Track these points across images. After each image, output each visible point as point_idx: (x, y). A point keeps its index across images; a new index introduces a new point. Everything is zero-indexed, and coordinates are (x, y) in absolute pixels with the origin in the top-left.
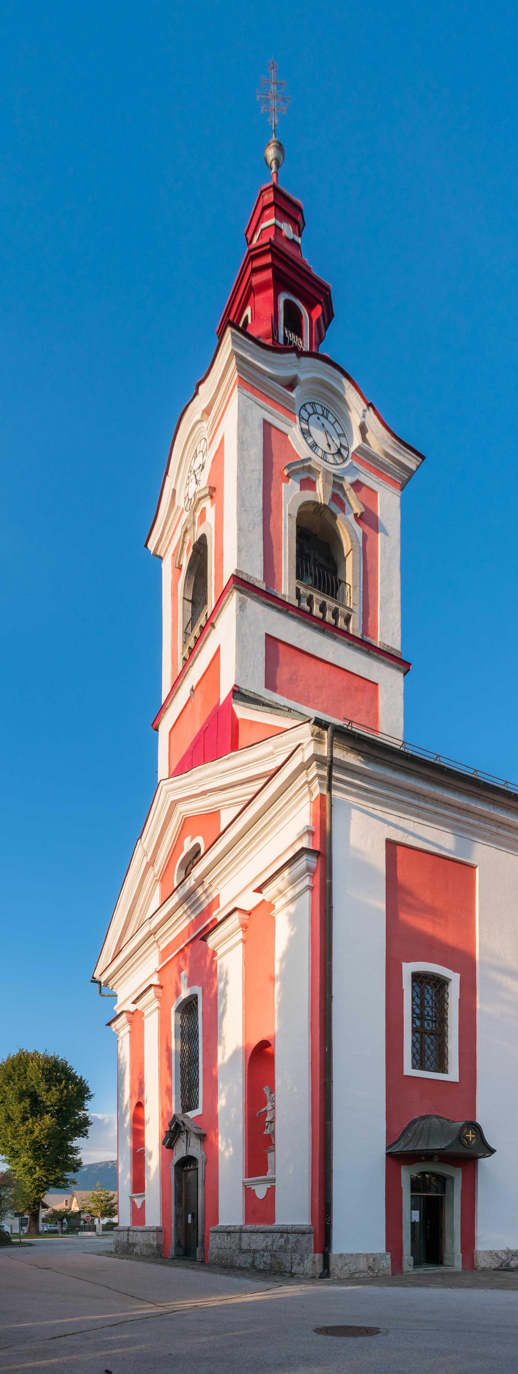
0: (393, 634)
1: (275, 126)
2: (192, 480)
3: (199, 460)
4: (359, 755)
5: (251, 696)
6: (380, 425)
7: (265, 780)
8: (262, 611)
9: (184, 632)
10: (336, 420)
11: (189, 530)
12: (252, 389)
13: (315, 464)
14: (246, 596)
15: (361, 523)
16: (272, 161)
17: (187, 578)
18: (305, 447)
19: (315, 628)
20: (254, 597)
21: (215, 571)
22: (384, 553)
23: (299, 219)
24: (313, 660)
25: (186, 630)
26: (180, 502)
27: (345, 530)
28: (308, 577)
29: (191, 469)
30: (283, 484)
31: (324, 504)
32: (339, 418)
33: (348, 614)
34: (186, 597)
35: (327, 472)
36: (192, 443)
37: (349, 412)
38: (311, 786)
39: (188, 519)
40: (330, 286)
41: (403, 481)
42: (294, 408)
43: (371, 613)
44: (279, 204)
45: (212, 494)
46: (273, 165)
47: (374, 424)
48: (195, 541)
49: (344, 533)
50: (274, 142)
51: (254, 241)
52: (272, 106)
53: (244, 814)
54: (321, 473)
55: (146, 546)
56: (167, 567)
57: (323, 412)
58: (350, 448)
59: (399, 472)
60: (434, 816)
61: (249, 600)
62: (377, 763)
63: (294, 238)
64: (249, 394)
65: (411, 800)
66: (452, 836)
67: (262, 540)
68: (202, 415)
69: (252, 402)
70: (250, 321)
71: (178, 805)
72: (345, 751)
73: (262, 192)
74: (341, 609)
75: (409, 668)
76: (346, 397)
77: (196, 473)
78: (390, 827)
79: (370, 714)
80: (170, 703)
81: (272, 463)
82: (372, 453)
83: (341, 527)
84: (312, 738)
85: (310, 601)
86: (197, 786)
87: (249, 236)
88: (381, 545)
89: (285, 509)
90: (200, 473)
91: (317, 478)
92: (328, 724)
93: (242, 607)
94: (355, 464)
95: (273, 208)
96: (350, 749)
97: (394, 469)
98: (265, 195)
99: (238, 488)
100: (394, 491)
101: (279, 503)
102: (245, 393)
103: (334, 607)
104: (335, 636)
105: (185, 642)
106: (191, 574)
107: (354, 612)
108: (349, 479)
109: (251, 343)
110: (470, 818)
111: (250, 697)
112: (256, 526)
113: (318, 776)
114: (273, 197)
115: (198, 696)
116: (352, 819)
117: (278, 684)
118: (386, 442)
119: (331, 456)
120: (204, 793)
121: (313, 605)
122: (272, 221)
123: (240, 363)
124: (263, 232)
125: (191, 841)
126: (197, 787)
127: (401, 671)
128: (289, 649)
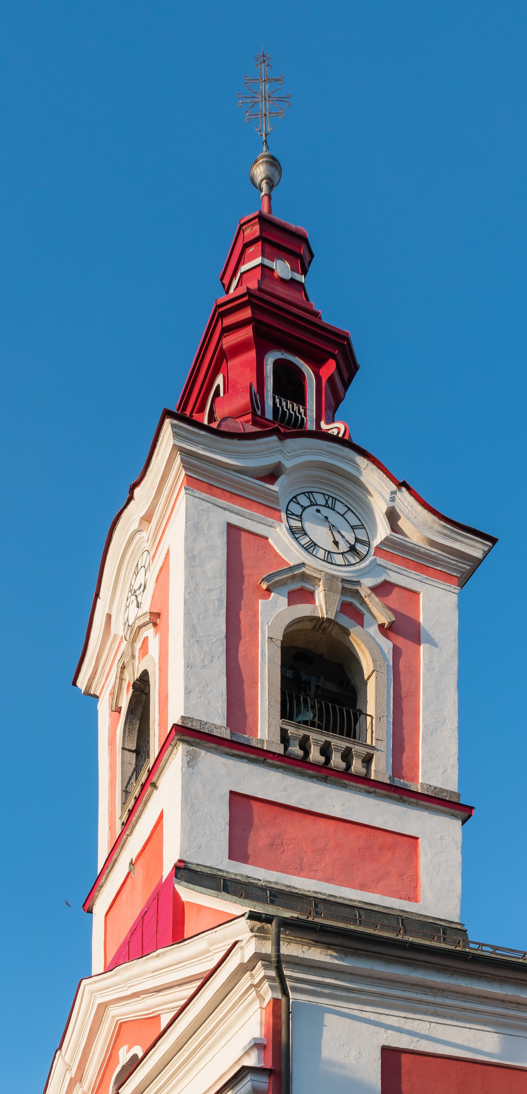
1: (266, 135)
2: (132, 601)
3: (140, 579)
4: (329, 948)
5: (205, 872)
6: (419, 508)
7: (198, 983)
9: (124, 791)
10: (349, 509)
11: (126, 666)
12: (210, 488)
13: (312, 569)
14: (198, 748)
15: (391, 634)
16: (262, 181)
17: (128, 724)
18: (297, 550)
19: (311, 777)
20: (211, 748)
21: (160, 716)
22: (429, 669)
23: (303, 251)
24: (309, 818)
25: (126, 787)
26: (118, 629)
27: (363, 646)
28: (308, 711)
29: (132, 588)
30: (260, 600)
31: (327, 618)
32: (354, 506)
33: (367, 753)
34: (126, 747)
35: (331, 578)
36: (131, 556)
37: (369, 497)
38: (259, 989)
39: (125, 652)
40: (348, 334)
42: (278, 504)
43: (407, 748)
44: (269, 237)
45: (155, 621)
46: (264, 185)
47: (409, 508)
48: (135, 679)
49: (362, 651)
50: (264, 157)
51: (232, 291)
52: (261, 111)
53: (177, 1024)
54: (322, 580)
55: (74, 683)
56: (104, 708)
57: (327, 501)
58: (371, 542)
59: (455, 562)
60: (462, 1013)
61: (203, 752)
62: (359, 956)
63: (293, 277)
64: (203, 495)
65: (420, 997)
66: (496, 1035)
67: (225, 675)
68: (140, 524)
69: (209, 504)
70: (222, 394)
71: (109, 1008)
72: (306, 945)
73: (241, 226)
74: (356, 748)
75: (471, 813)
76: (363, 479)
77: (137, 593)
78: (389, 1032)
79: (405, 877)
80: (106, 880)
81: (242, 577)
82: (408, 544)
83: (358, 644)
84: (251, 934)
85: (304, 744)
86: (126, 986)
87: (226, 282)
88: (424, 659)
90: (142, 593)
91: (316, 587)
92: (271, 917)
93: (191, 762)
94: (380, 561)
95: (260, 243)
96: (313, 943)
97: (447, 560)
98: (246, 229)
99: (185, 614)
100: (448, 588)
101: (254, 625)
102: (197, 495)
104: (344, 783)
105: (124, 804)
106: (133, 718)
107: (378, 750)
108: (368, 582)
109: (203, 433)
110: (523, 1011)
111: (203, 872)
112: (215, 659)
113: (265, 977)
114: (258, 230)
115: (139, 871)
116: (326, 1026)
117: (250, 852)
118: (432, 528)
119: (341, 556)
120: (136, 995)
121: (310, 748)
122: (258, 261)
123: (188, 459)
124: (244, 276)
125: (128, 1051)
126: (126, 988)
127: (458, 818)
128: (269, 806)
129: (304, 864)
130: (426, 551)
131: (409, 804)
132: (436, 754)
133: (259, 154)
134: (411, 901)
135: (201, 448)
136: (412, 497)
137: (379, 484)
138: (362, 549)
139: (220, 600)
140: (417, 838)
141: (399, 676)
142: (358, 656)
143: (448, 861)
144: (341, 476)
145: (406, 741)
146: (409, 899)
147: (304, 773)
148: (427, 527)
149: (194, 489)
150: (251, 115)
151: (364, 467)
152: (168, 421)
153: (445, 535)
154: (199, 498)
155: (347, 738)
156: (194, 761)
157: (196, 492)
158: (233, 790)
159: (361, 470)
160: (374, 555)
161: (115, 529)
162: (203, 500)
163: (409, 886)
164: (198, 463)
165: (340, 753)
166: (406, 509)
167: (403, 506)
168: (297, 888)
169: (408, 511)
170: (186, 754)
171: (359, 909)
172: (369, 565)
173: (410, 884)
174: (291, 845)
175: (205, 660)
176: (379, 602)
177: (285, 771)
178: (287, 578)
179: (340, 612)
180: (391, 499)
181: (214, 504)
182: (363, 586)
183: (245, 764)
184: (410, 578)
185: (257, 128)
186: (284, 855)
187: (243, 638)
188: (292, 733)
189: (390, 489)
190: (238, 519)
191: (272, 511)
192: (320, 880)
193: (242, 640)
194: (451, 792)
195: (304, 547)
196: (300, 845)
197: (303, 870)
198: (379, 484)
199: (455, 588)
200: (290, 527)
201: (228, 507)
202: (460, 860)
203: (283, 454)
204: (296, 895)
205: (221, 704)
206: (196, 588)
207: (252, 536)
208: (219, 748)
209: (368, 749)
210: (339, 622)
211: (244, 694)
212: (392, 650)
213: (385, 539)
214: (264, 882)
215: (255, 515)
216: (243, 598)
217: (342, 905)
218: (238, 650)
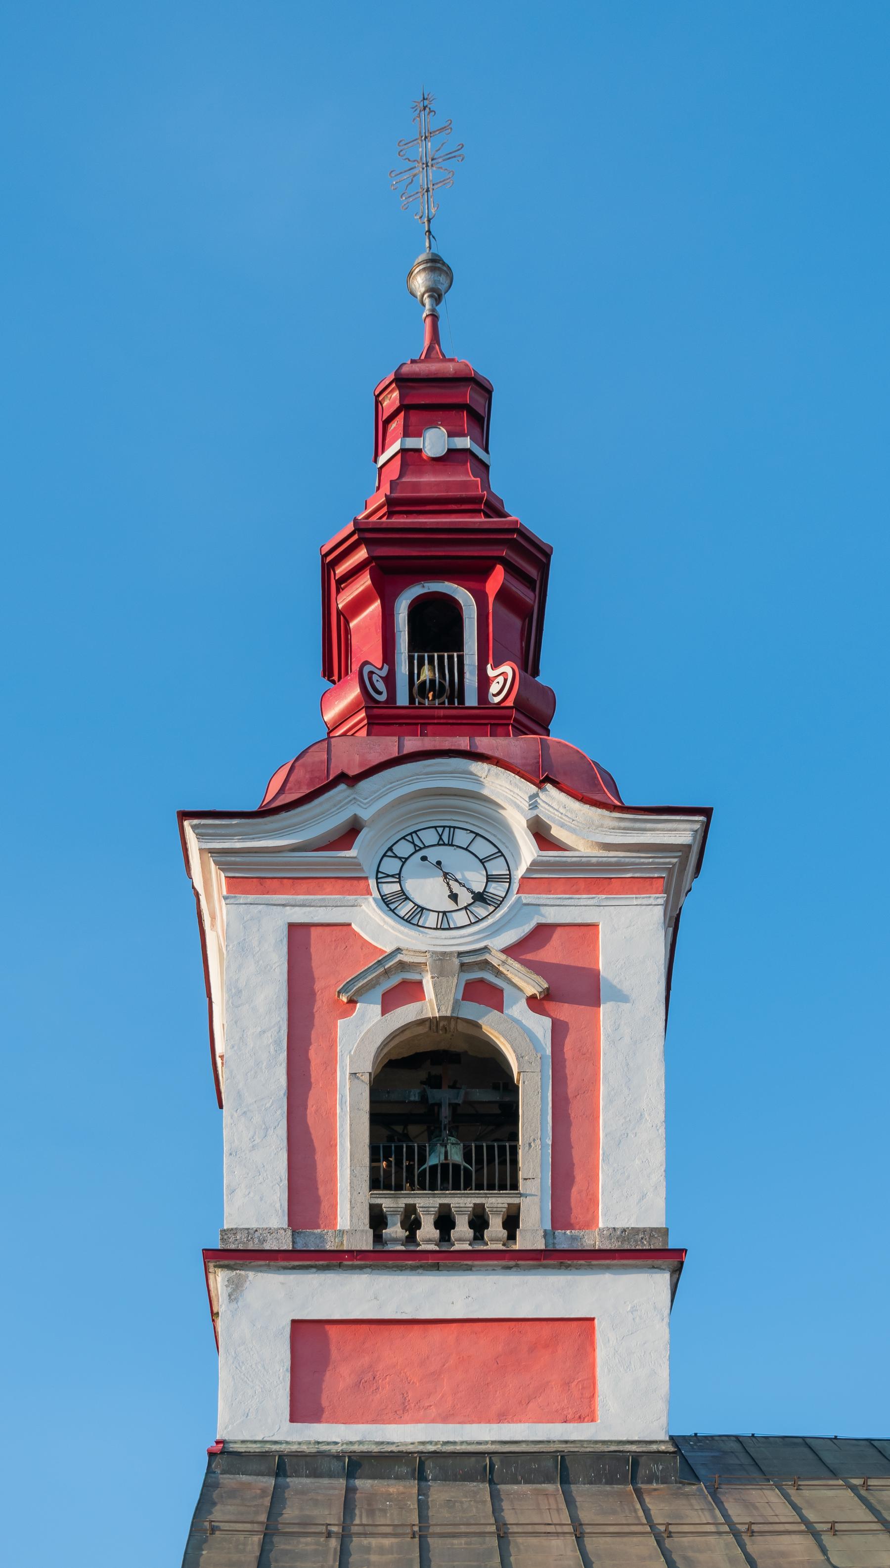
0: (644, 1196)
1: (429, 221)
8: (282, 1284)
10: (477, 834)
14: (243, 1270)
16: (423, 295)
18: (393, 928)
19: (414, 1268)
20: (260, 1266)
24: (416, 1327)
35: (442, 957)
37: (501, 811)
41: (670, 871)
42: (362, 870)
43: (579, 1175)
47: (562, 810)
59: (651, 860)
61: (251, 1274)
64: (251, 898)
69: (260, 907)
73: (377, 397)
76: (486, 792)
81: (313, 994)
89: (342, 1068)
94: (526, 898)
97: (637, 860)
98: (384, 399)
100: (645, 902)
101: (330, 1063)
102: (241, 901)
103: (472, 1205)
104: (467, 1265)
109: (235, 821)
111: (249, 1452)
112: (271, 1132)
117: (325, 1403)
118: (602, 826)
123: (223, 859)
127: (664, 1269)
128: (354, 1327)
129: (409, 1400)
130: (601, 859)
131: (577, 1269)
132: (626, 1174)
133: (415, 260)
134: (583, 1422)
135: (238, 839)
136: (563, 793)
137: (511, 791)
138: (498, 890)
139: (277, 1043)
140: (593, 1319)
141: (564, 1067)
142: (503, 1051)
143: (644, 1344)
144: (455, 795)
145: (576, 1167)
146: (581, 1419)
147: (402, 1266)
148: (594, 828)
149: (236, 895)
150: (409, 197)
151: (484, 775)
152: (186, 823)
153: (624, 829)
154: (245, 904)
155: (477, 1192)
156: (238, 1291)
157: (240, 898)
158: (296, 1318)
159: (482, 779)
160: (517, 893)
161: (204, 920)
162: (251, 904)
163: (581, 1398)
164: (238, 859)
165: (467, 1215)
166: (556, 813)
167: (551, 810)
168: (393, 1443)
169: (560, 815)
170: (227, 1283)
171: (491, 1455)
172: (509, 911)
173: (582, 1394)
174: (388, 1377)
175: (254, 1138)
176: (521, 968)
177: (374, 1269)
178: (378, 977)
179: (464, 998)
180: (531, 807)
181: (267, 904)
182: (494, 952)
183: (313, 1276)
184: (581, 906)
185: (416, 215)
186: (378, 1395)
187: (313, 1085)
188: (388, 1208)
189: (527, 794)
190: (305, 913)
191: (356, 882)
192: (433, 1421)
193: (312, 1088)
194: (652, 1229)
195: (404, 920)
196: (402, 1374)
197: (408, 1410)
198: (511, 791)
199: (658, 898)
200: (382, 896)
201: (287, 902)
202: (667, 1336)
203: (359, 803)
204: (391, 1454)
205: (278, 1196)
206: (243, 1035)
207: (327, 929)
208: (272, 1263)
209: (510, 1199)
210: (460, 1016)
211: (316, 1169)
212: (550, 1031)
213: (531, 865)
214: (342, 1445)
215: (328, 898)
216: (314, 1025)
217: (463, 1455)
218: (307, 1105)
